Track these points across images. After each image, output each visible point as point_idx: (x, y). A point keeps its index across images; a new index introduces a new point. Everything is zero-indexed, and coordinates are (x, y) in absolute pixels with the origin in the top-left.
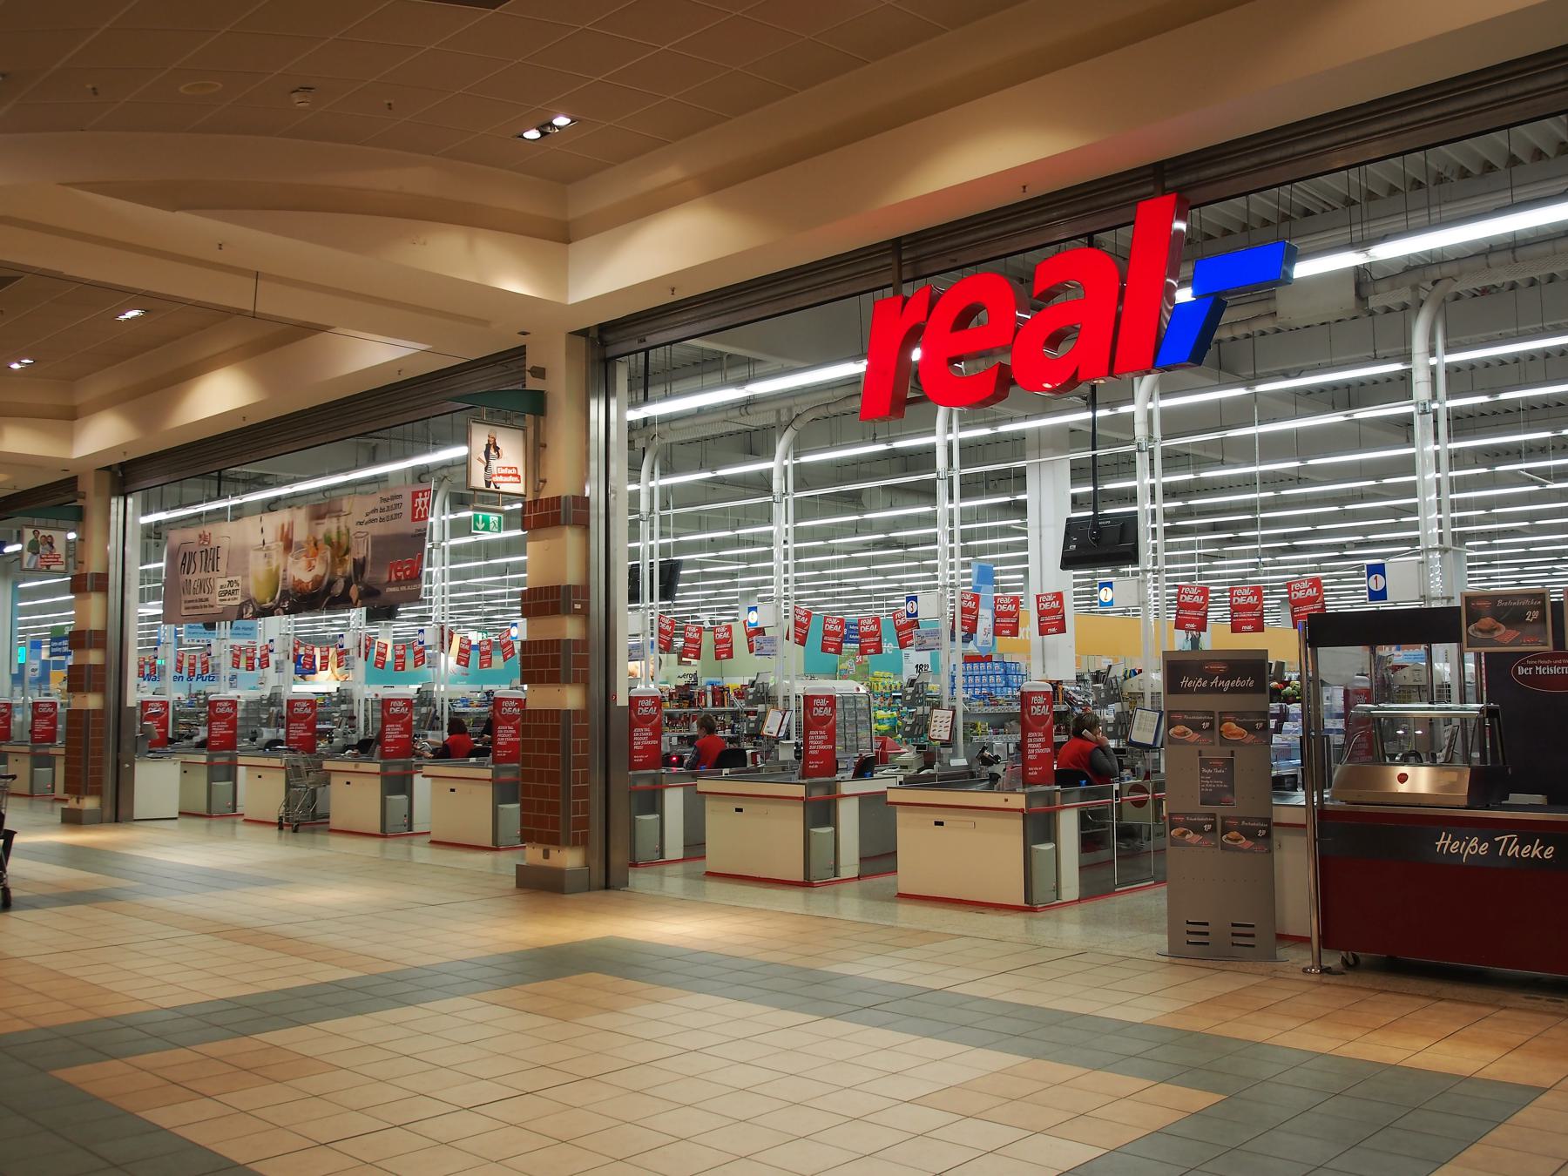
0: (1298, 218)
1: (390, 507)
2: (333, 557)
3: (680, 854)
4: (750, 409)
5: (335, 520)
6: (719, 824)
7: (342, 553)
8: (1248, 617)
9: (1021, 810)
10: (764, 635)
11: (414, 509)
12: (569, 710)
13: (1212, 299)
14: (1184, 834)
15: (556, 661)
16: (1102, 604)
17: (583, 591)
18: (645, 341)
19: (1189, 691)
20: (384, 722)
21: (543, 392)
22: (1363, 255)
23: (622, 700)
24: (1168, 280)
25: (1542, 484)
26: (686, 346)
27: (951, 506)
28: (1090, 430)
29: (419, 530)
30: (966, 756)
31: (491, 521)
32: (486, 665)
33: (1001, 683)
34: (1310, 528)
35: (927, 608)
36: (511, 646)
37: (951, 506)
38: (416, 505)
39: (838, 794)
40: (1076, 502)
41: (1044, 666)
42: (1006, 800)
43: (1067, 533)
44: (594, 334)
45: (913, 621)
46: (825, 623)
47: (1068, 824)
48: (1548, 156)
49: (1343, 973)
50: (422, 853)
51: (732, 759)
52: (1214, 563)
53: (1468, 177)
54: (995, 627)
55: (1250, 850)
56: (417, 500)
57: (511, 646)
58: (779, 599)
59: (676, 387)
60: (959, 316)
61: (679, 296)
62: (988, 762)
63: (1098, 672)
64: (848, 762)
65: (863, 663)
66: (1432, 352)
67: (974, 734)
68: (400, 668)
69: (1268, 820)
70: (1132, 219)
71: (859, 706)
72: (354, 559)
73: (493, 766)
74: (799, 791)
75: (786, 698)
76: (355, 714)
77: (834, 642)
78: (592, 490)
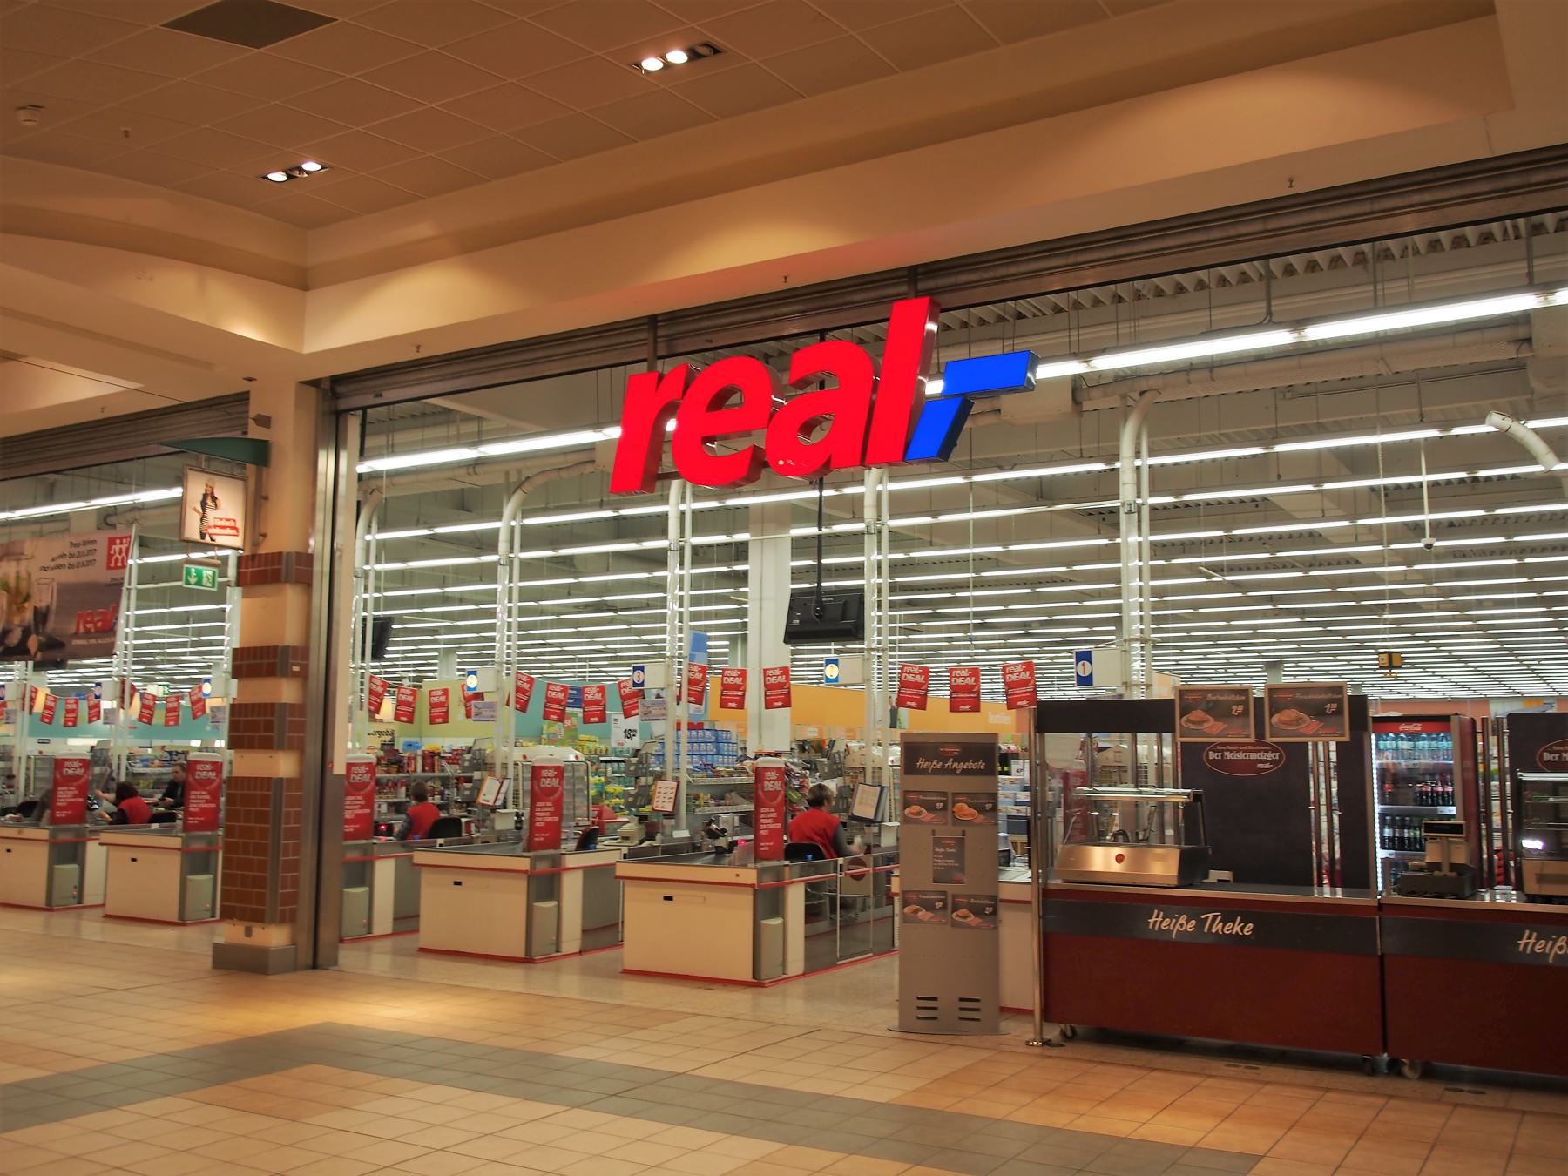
0: (1011, 320)
1: (81, 552)
2: (10, 604)
3: (388, 929)
4: (478, 469)
5: (13, 564)
6: (435, 897)
7: (20, 600)
8: (966, 697)
9: (752, 886)
10: (483, 700)
11: (110, 556)
12: (282, 778)
13: (960, 399)
14: (916, 911)
15: (269, 726)
16: (828, 680)
17: (303, 652)
18: (381, 396)
19: (924, 772)
20: (56, 783)
21: (267, 441)
22: (1085, 365)
23: (339, 768)
24: (920, 378)
25: (1209, 576)
26: (426, 403)
27: (682, 572)
28: (817, 508)
29: (115, 579)
30: (689, 827)
31: (204, 575)
32: (171, 723)
33: (712, 751)
34: (1002, 608)
35: (654, 677)
36: (202, 703)
37: (682, 572)
38: (112, 552)
39: (563, 867)
40: (797, 574)
41: (760, 736)
42: (738, 875)
43: (791, 608)
44: (326, 385)
45: (639, 690)
46: (548, 690)
47: (796, 898)
48: (1230, 283)
49: (1062, 1046)
50: (92, 928)
51: (447, 829)
52: (911, 637)
53: (1161, 296)
54: (722, 700)
55: (977, 927)
56: (114, 547)
57: (202, 703)
58: (500, 664)
59: (399, 438)
60: (713, 398)
61: (424, 354)
62: (714, 835)
63: (804, 741)
64: (570, 832)
65: (573, 727)
66: (1138, 455)
67: (697, 806)
68: (70, 724)
69: (994, 898)
70: (887, 316)
71: (577, 774)
72: (36, 608)
73: (183, 835)
74: (524, 864)
75: (505, 766)
76: (15, 773)
77: (555, 710)
78: (317, 543)
